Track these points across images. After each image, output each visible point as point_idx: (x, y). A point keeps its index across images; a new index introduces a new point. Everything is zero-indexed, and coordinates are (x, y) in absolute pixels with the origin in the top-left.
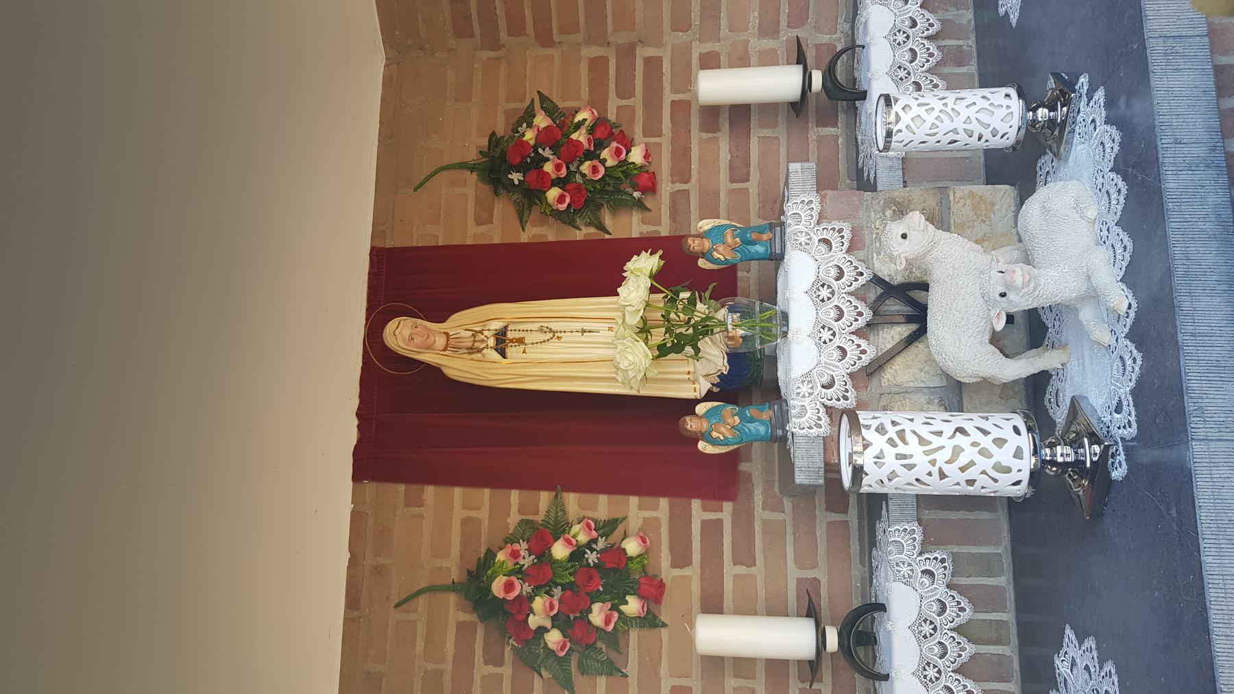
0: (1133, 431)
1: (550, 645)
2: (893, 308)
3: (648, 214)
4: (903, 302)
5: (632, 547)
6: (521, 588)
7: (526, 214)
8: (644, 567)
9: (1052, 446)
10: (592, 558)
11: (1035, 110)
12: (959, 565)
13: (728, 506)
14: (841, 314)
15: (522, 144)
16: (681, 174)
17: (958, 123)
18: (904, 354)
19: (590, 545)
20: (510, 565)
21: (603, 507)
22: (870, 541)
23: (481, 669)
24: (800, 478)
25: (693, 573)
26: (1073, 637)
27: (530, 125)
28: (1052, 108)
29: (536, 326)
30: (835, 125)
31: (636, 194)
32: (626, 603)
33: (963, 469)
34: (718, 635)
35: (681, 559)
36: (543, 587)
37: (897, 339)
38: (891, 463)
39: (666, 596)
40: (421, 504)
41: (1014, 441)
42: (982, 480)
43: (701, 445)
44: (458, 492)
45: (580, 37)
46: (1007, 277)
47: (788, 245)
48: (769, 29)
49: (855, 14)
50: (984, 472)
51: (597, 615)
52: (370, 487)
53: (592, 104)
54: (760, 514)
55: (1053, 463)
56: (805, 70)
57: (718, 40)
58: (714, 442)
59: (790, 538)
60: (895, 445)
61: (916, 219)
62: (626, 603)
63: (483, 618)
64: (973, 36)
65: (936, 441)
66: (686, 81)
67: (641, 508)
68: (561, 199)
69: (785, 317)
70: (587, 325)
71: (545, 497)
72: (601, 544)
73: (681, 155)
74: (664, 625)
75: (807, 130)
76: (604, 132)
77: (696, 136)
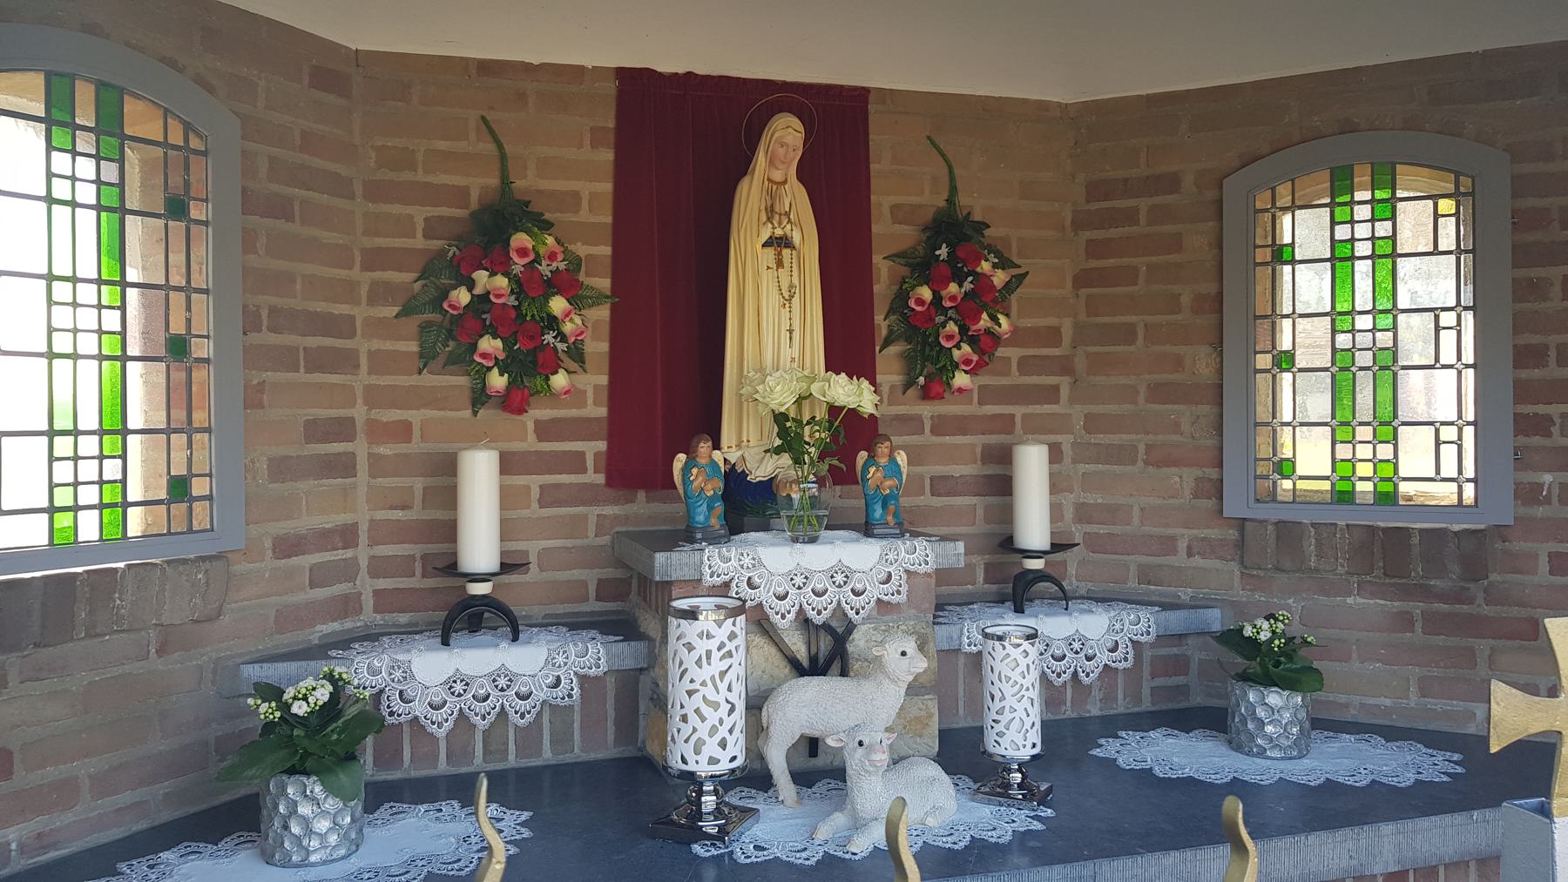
0: (742, 860)
1: (454, 294)
2: (822, 644)
3: (900, 391)
4: (828, 652)
5: (560, 380)
6: (519, 264)
7: (902, 261)
8: (538, 392)
9: (716, 792)
10: (549, 338)
11: (1019, 770)
12: (557, 711)
13: (600, 479)
14: (818, 594)
15: (979, 258)
16: (942, 426)
17: (1010, 701)
18: (779, 655)
19: (562, 337)
20: (542, 250)
21: (598, 348)
22: (576, 625)
23: (420, 214)
24: (660, 558)
25: (530, 443)
26: (523, 818)
27: (995, 266)
28: (1020, 786)
29: (796, 281)
30: (986, 581)
31: (921, 380)
32: (501, 375)
33: (697, 711)
34: (480, 475)
35: (545, 430)
36: (520, 287)
37: (793, 648)
38: (702, 646)
39: (507, 415)
40: (594, 145)
41: (724, 757)
42: (687, 730)
43: (682, 457)
44: (608, 187)
45: (1082, 317)
46: (878, 747)
47: (885, 542)
48: (1084, 513)
49: (1097, 600)
50: (695, 730)
51: (490, 345)
52: (611, 87)
53: (1015, 330)
54: (595, 511)
55: (700, 793)
56: (1045, 553)
57: (1074, 462)
58: (686, 470)
59: (569, 543)
60: (719, 649)
61: (921, 664)
62: (501, 375)
63: (472, 214)
64: (1074, 715)
65: (723, 686)
66: (1036, 429)
67: (596, 387)
68: (920, 302)
69: (813, 540)
70: (796, 335)
71: (604, 283)
72: (561, 346)
73: (961, 425)
74: (475, 413)
75: (981, 552)
76: (986, 344)
77: (977, 441)
